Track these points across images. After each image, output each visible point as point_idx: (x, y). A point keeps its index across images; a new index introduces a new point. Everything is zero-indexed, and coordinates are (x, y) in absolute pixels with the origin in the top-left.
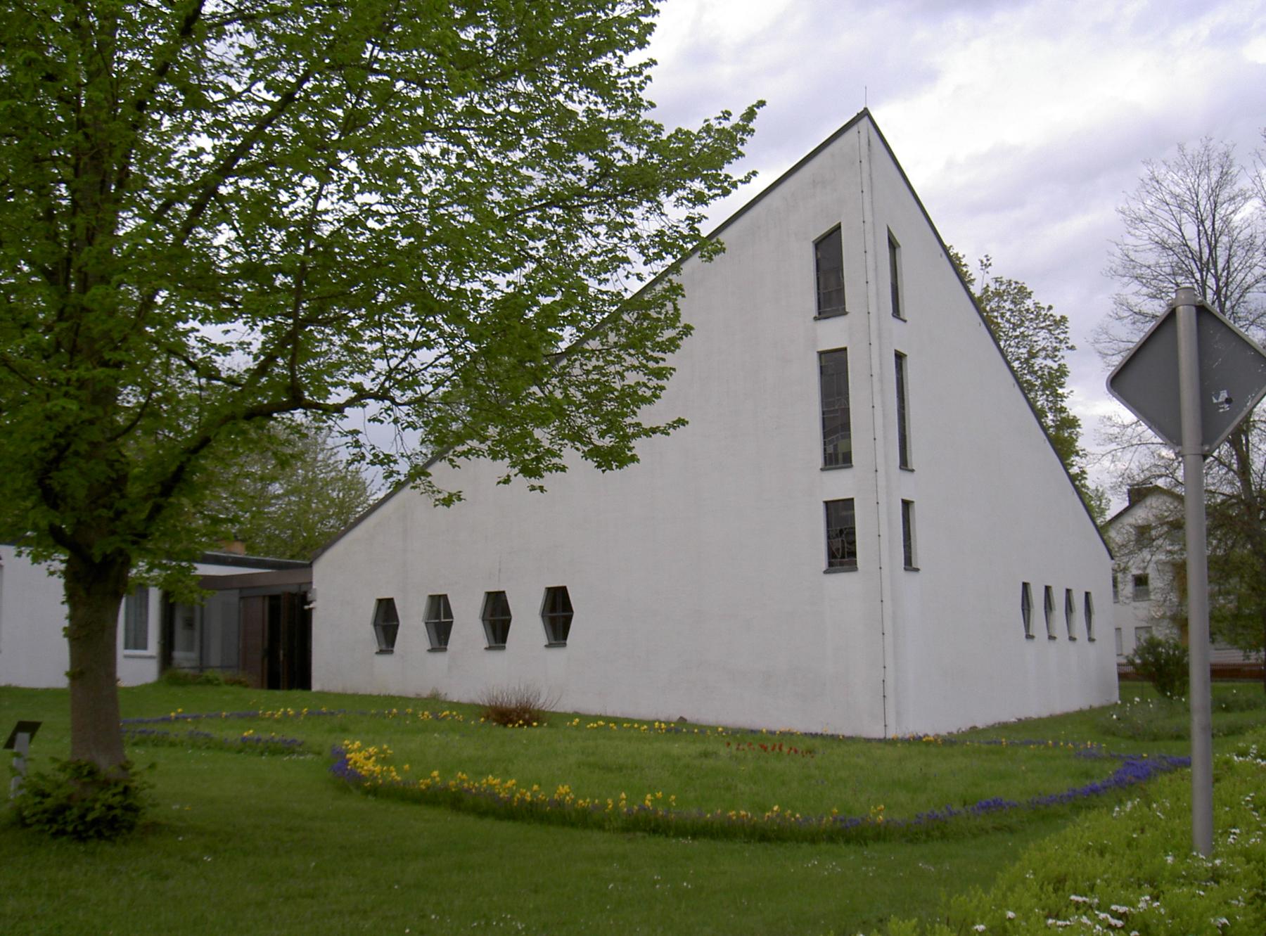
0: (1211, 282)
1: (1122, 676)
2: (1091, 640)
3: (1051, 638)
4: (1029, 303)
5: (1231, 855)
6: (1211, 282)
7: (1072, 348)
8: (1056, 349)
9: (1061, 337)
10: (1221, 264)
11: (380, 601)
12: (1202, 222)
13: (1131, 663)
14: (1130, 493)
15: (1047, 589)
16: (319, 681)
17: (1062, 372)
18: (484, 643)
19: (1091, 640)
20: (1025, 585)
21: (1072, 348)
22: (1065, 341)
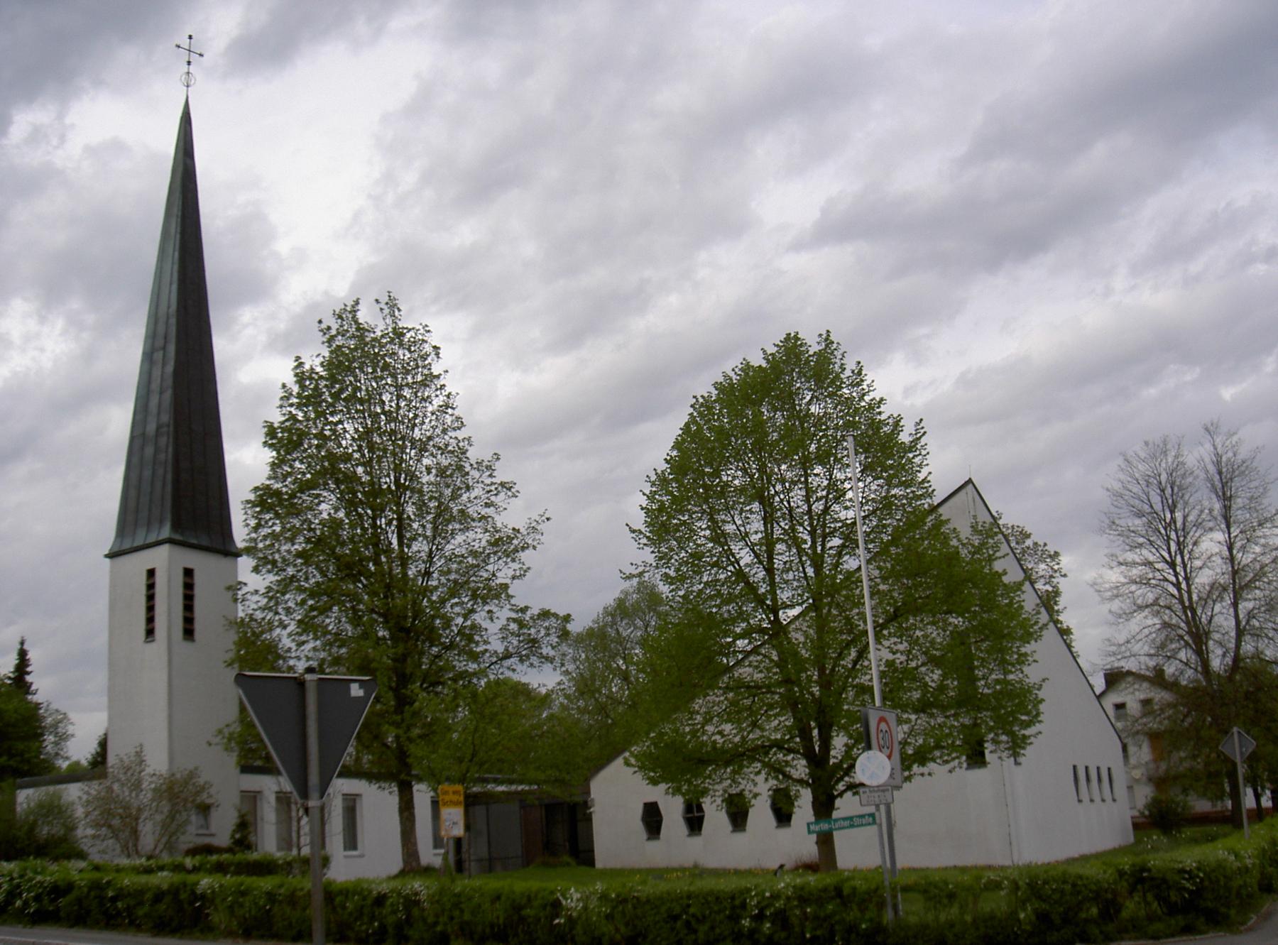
0: (1173, 535)
1: (1136, 826)
2: (1114, 800)
3: (1092, 801)
4: (1029, 542)
5: (1101, 932)
6: (1173, 535)
7: (1065, 576)
8: (1051, 577)
9: (1056, 567)
10: (1179, 524)
11: (646, 805)
12: (1163, 491)
13: (1142, 813)
14: (1106, 676)
15: (1087, 768)
16: (603, 857)
17: (1057, 593)
18: (730, 828)
19: (1114, 800)
20: (1075, 767)
21: (1065, 576)
22: (1059, 570)
